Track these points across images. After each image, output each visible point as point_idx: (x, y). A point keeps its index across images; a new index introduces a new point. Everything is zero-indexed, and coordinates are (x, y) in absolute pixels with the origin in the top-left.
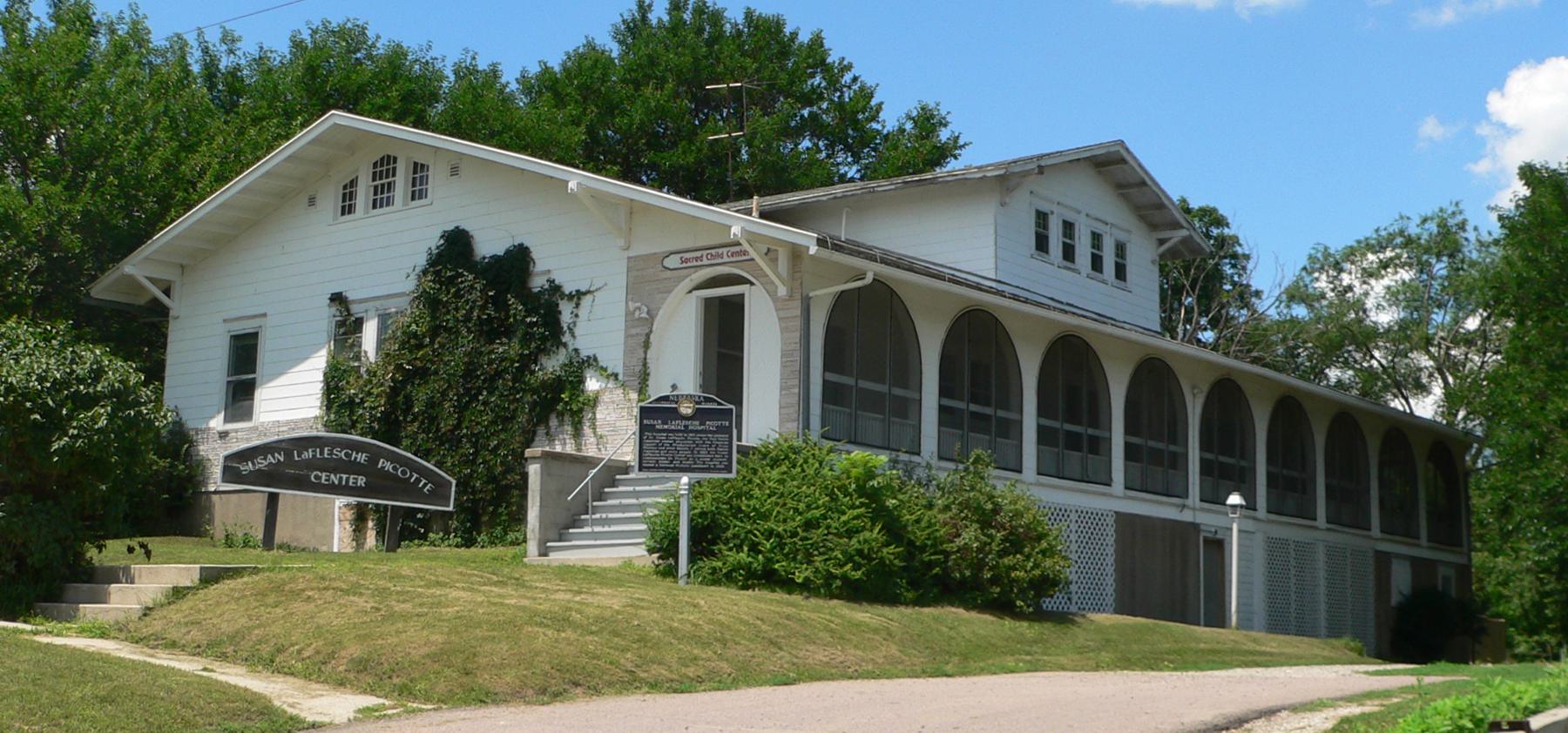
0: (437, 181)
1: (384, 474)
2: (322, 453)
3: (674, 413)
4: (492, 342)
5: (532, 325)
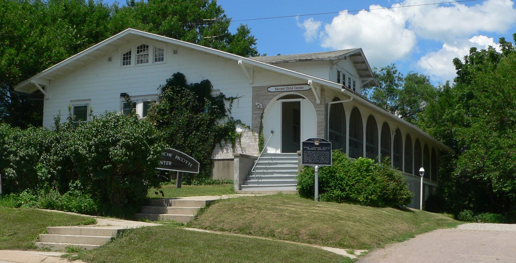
0: (168, 56)
4: (197, 114)
5: (215, 108)
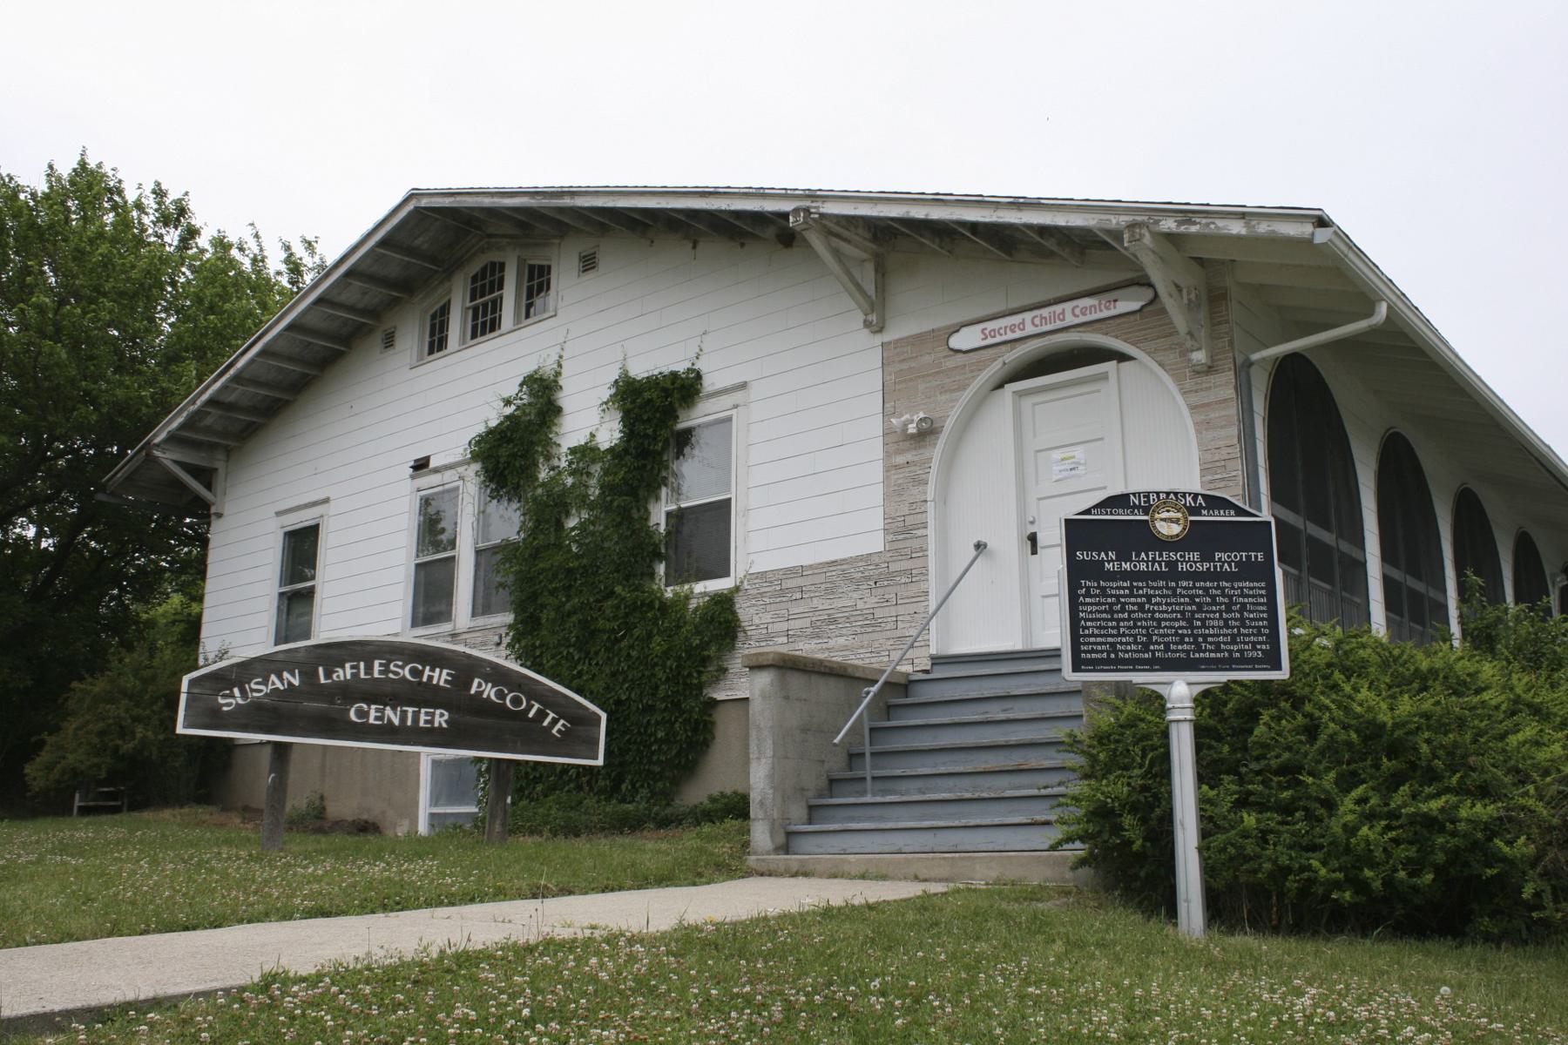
1: (482, 707)
2: (369, 669)
3: (1139, 537)
